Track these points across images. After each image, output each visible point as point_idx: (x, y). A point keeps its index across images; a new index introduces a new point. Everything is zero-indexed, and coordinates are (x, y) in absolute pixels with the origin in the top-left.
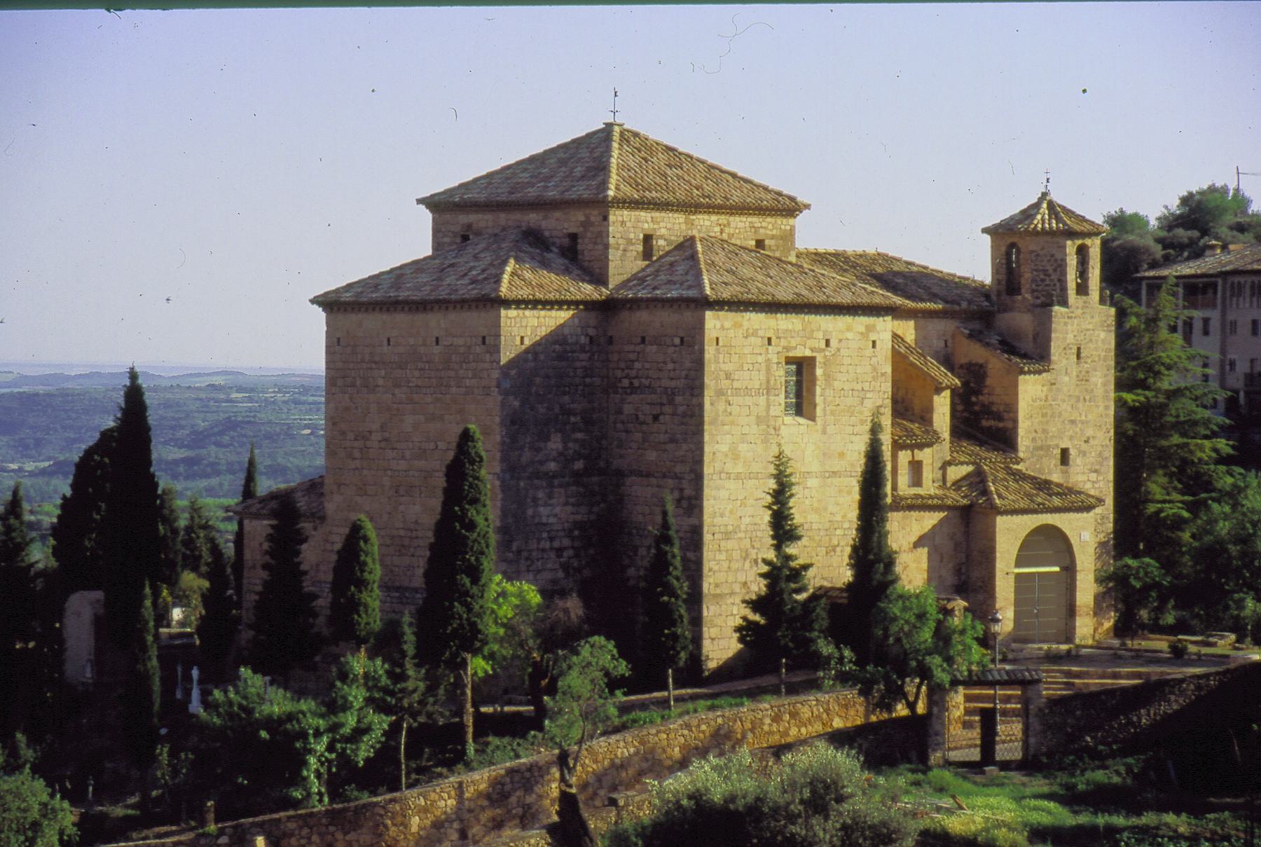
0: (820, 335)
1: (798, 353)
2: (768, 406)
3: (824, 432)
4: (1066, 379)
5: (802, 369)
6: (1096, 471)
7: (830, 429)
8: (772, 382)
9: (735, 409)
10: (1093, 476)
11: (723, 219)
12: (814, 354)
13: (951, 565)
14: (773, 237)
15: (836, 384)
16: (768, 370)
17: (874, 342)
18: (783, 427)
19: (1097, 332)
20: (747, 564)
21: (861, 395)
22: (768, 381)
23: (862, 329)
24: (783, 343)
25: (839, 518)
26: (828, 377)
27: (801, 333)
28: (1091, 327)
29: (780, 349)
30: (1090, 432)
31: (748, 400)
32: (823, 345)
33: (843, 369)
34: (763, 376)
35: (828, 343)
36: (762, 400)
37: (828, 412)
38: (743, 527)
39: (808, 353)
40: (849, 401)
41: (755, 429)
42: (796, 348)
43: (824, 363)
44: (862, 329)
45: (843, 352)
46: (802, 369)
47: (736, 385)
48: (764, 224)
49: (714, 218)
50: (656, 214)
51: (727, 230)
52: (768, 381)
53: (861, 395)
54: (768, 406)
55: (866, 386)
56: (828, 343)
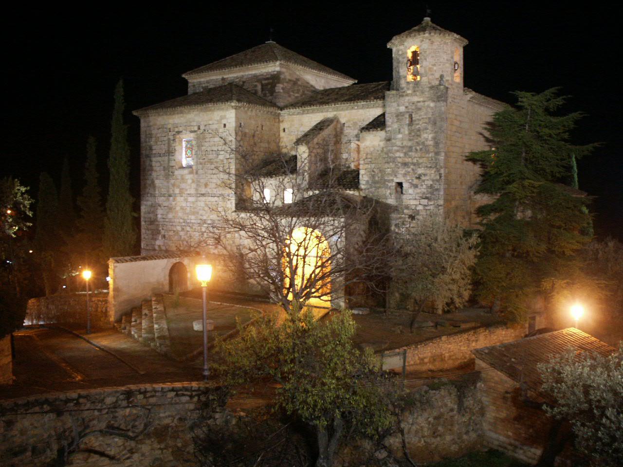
6: (426, 198)
8: (171, 149)
10: (425, 202)
15: (203, 148)
19: (426, 103)
30: (420, 171)
32: (196, 128)
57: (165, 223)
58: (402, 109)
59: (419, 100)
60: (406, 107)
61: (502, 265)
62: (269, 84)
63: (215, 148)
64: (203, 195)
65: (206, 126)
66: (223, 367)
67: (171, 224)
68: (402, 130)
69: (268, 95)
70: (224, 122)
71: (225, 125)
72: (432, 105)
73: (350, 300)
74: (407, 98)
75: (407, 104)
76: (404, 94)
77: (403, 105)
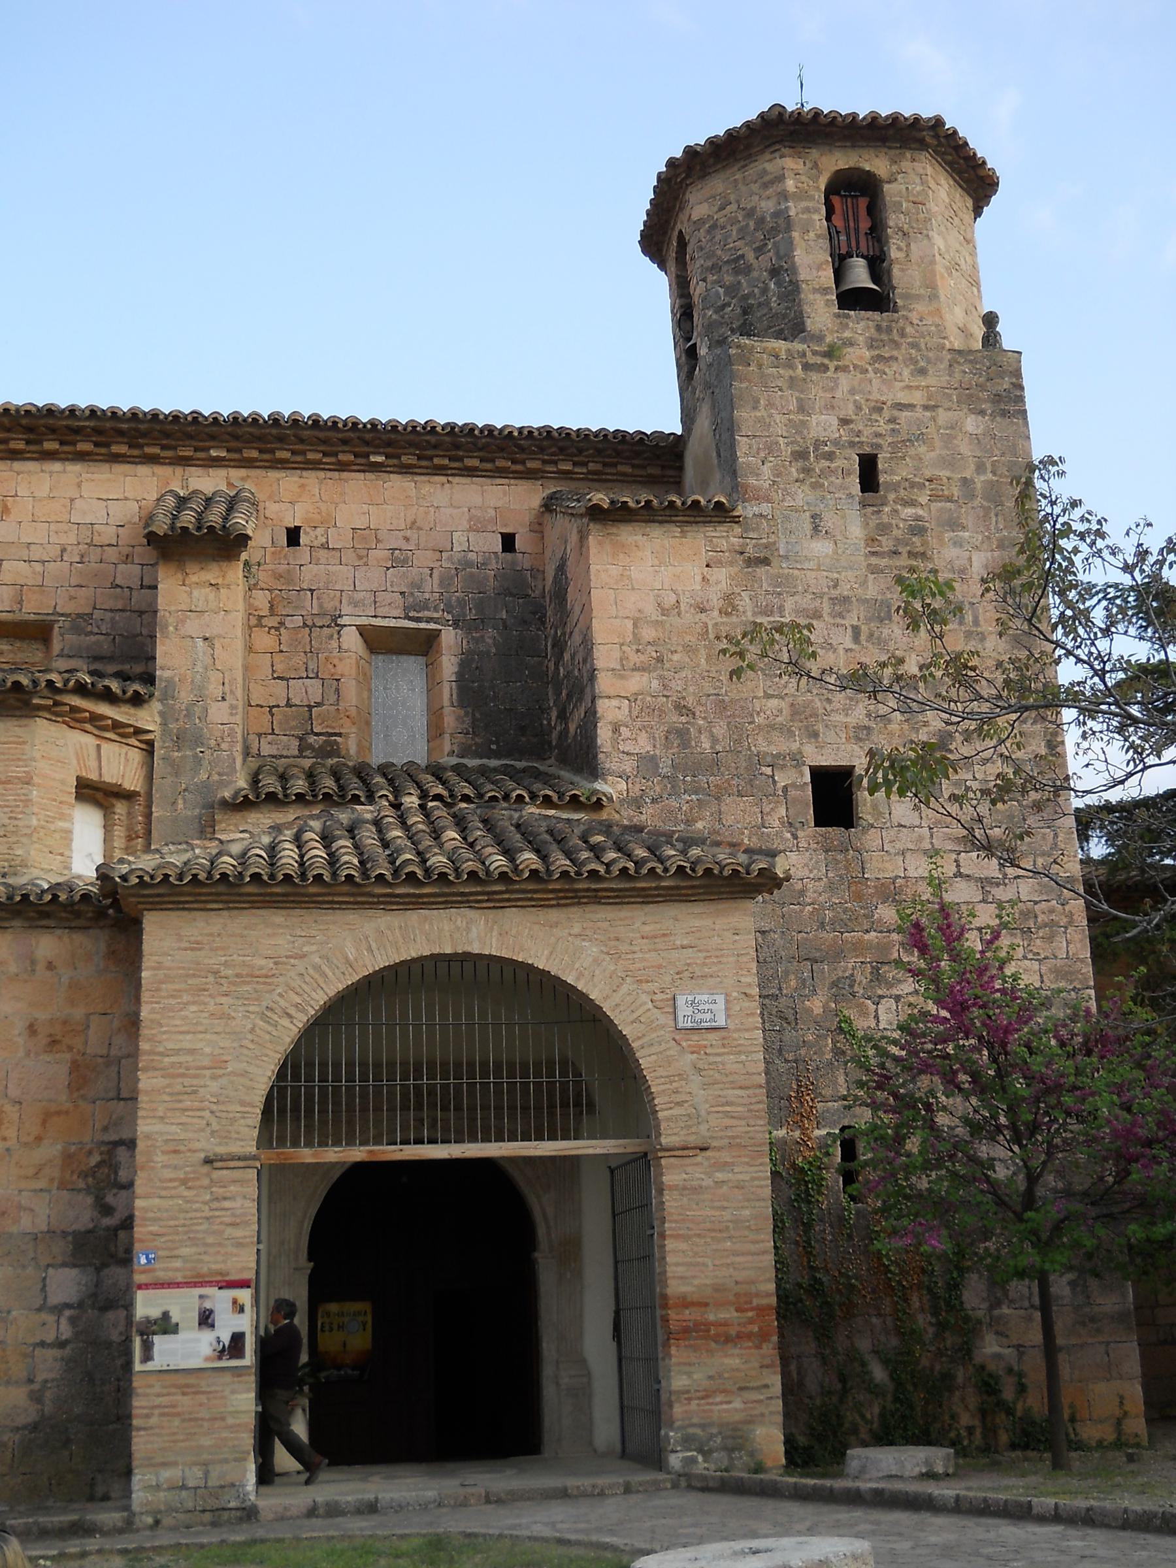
4: (821, 548)
13: (51, 1150)
19: (943, 416)
28: (917, 398)
58: (823, 425)
60: (844, 422)
68: (830, 521)
72: (972, 424)
77: (830, 407)
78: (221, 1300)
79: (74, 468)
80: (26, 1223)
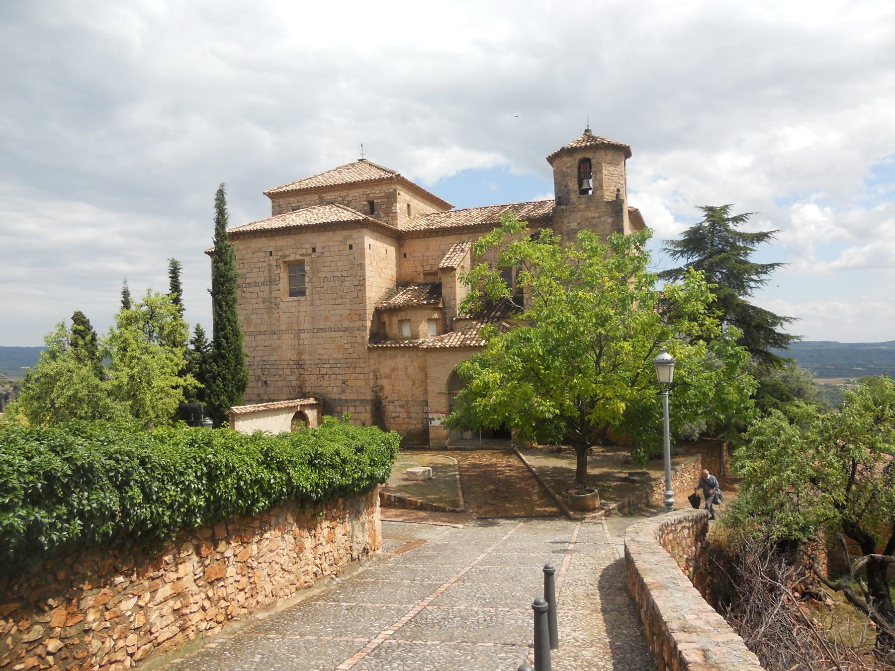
0: (308, 246)
1: (292, 258)
2: (270, 292)
3: (312, 305)
5: (296, 268)
7: (316, 303)
8: (273, 277)
9: (248, 295)
11: (344, 193)
12: (303, 258)
14: (380, 197)
15: (321, 275)
16: (270, 271)
17: (351, 247)
18: (281, 303)
19: (602, 219)
20: (260, 384)
21: (342, 279)
22: (270, 277)
23: (342, 239)
24: (280, 253)
25: (325, 357)
26: (315, 271)
27: (294, 247)
29: (278, 257)
31: (256, 289)
32: (310, 251)
33: (326, 264)
34: (266, 274)
35: (314, 250)
36: (267, 288)
37: (314, 292)
38: (256, 363)
39: (299, 257)
40: (332, 284)
41: (262, 306)
42: (289, 255)
43: (311, 262)
44: (342, 239)
45: (326, 254)
46: (296, 268)
47: (247, 281)
48: (373, 191)
49: (337, 194)
50: (300, 198)
51: (347, 199)
52: (270, 277)
53: (342, 279)
54: (270, 292)
55: (345, 274)
56: (314, 250)
57: (267, 367)
59: (593, 215)
61: (756, 382)
62: (383, 203)
63: (339, 274)
64: (321, 330)
65: (323, 248)
66: (795, 634)
67: (276, 367)
69: (382, 215)
70: (350, 242)
71: (351, 247)
73: (661, 450)
74: (579, 214)
75: (579, 221)
76: (576, 210)
78: (441, 415)
79: (440, 238)
80: (420, 399)
